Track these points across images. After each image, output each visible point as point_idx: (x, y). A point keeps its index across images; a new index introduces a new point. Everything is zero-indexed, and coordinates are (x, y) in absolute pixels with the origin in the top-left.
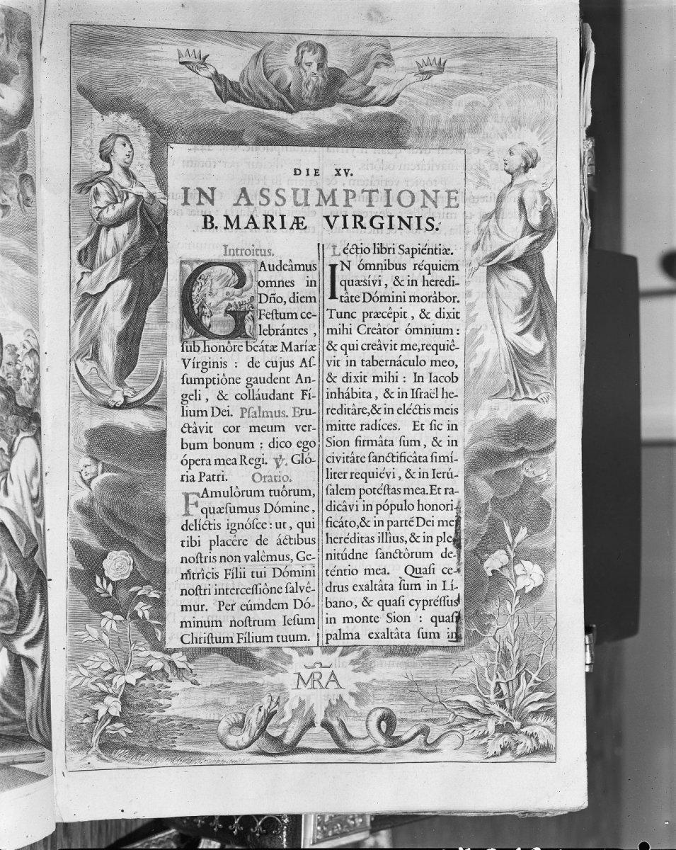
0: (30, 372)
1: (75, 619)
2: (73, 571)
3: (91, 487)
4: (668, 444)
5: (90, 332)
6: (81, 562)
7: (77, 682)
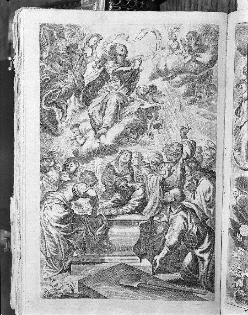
0: (207, 156)
1: (230, 248)
2: (230, 229)
3: (237, 200)
5: (238, 141)
6: (233, 227)
7: (230, 271)
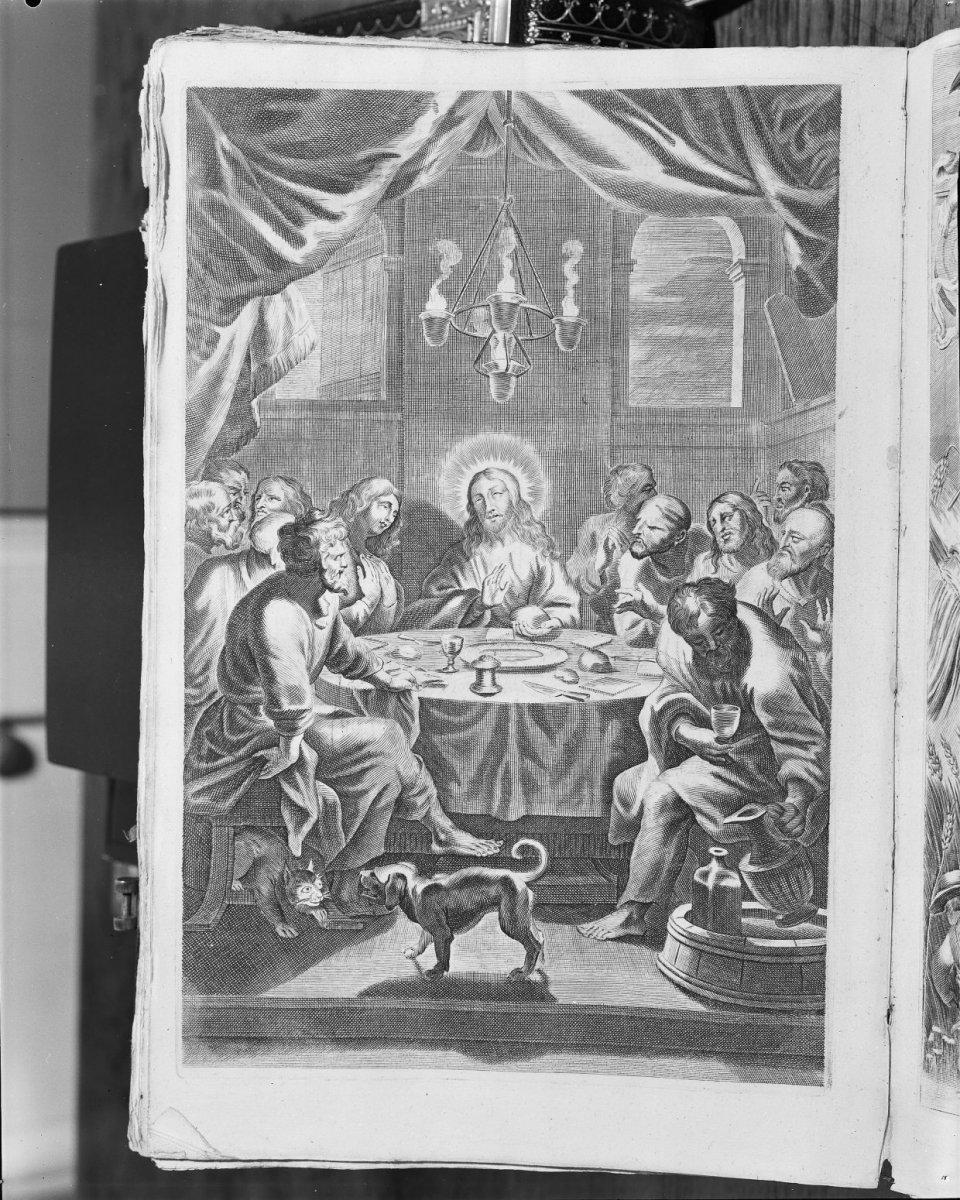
4: (8, 512)
6: (725, 887)
